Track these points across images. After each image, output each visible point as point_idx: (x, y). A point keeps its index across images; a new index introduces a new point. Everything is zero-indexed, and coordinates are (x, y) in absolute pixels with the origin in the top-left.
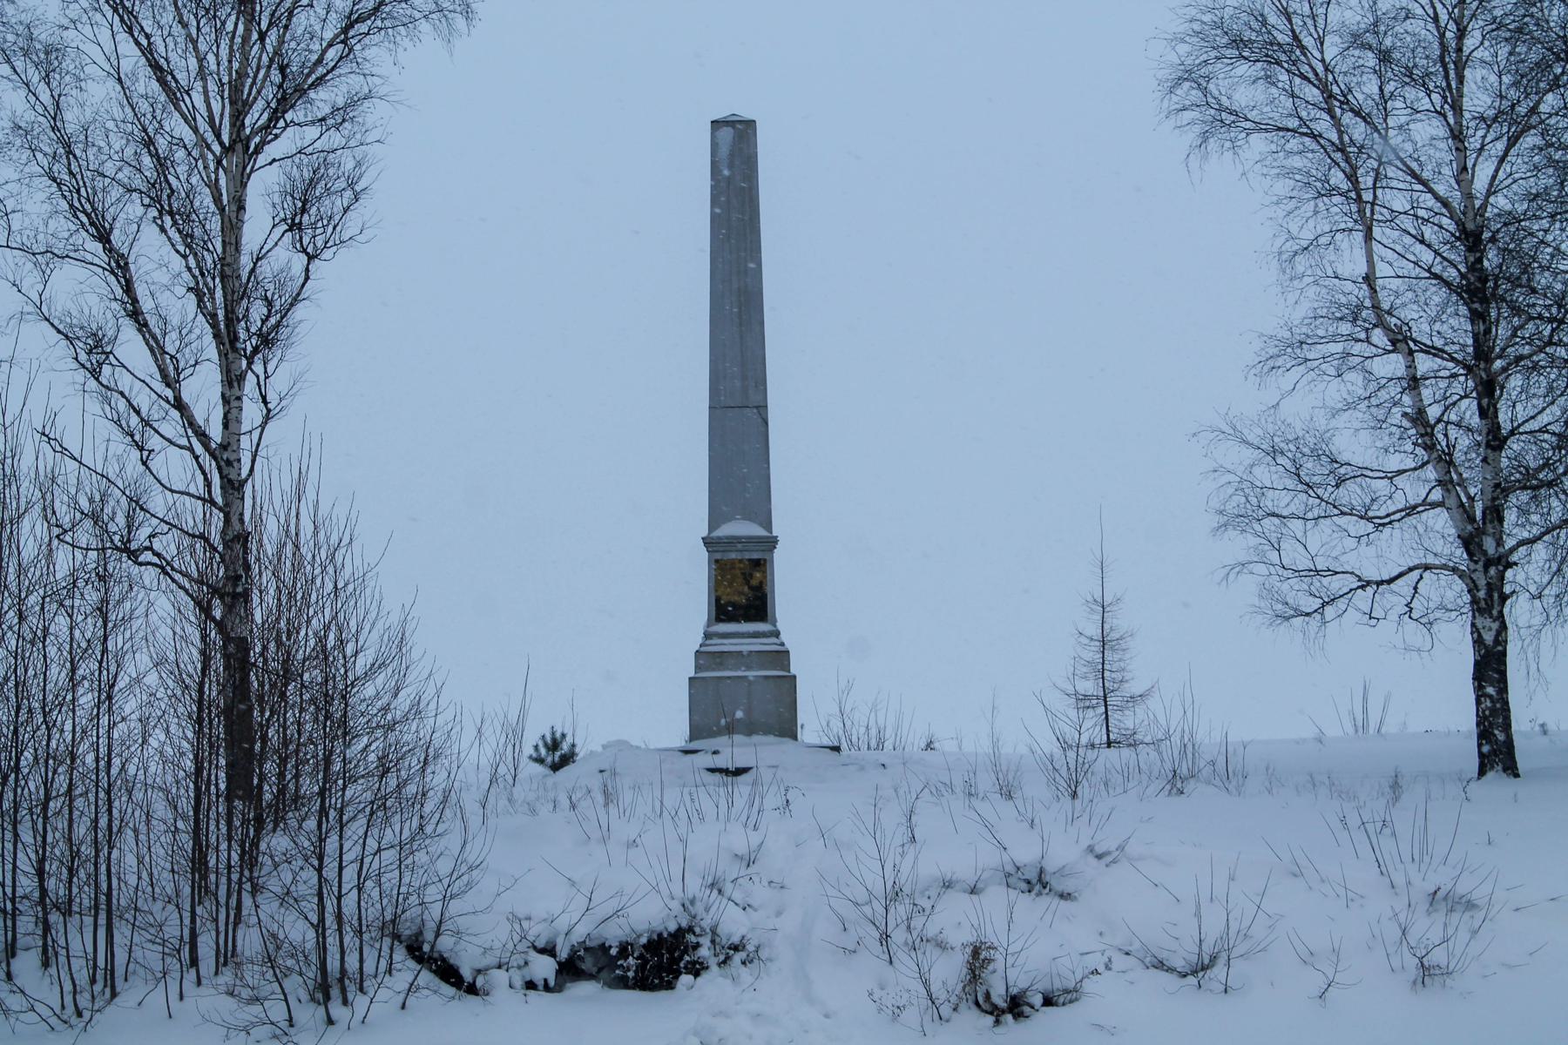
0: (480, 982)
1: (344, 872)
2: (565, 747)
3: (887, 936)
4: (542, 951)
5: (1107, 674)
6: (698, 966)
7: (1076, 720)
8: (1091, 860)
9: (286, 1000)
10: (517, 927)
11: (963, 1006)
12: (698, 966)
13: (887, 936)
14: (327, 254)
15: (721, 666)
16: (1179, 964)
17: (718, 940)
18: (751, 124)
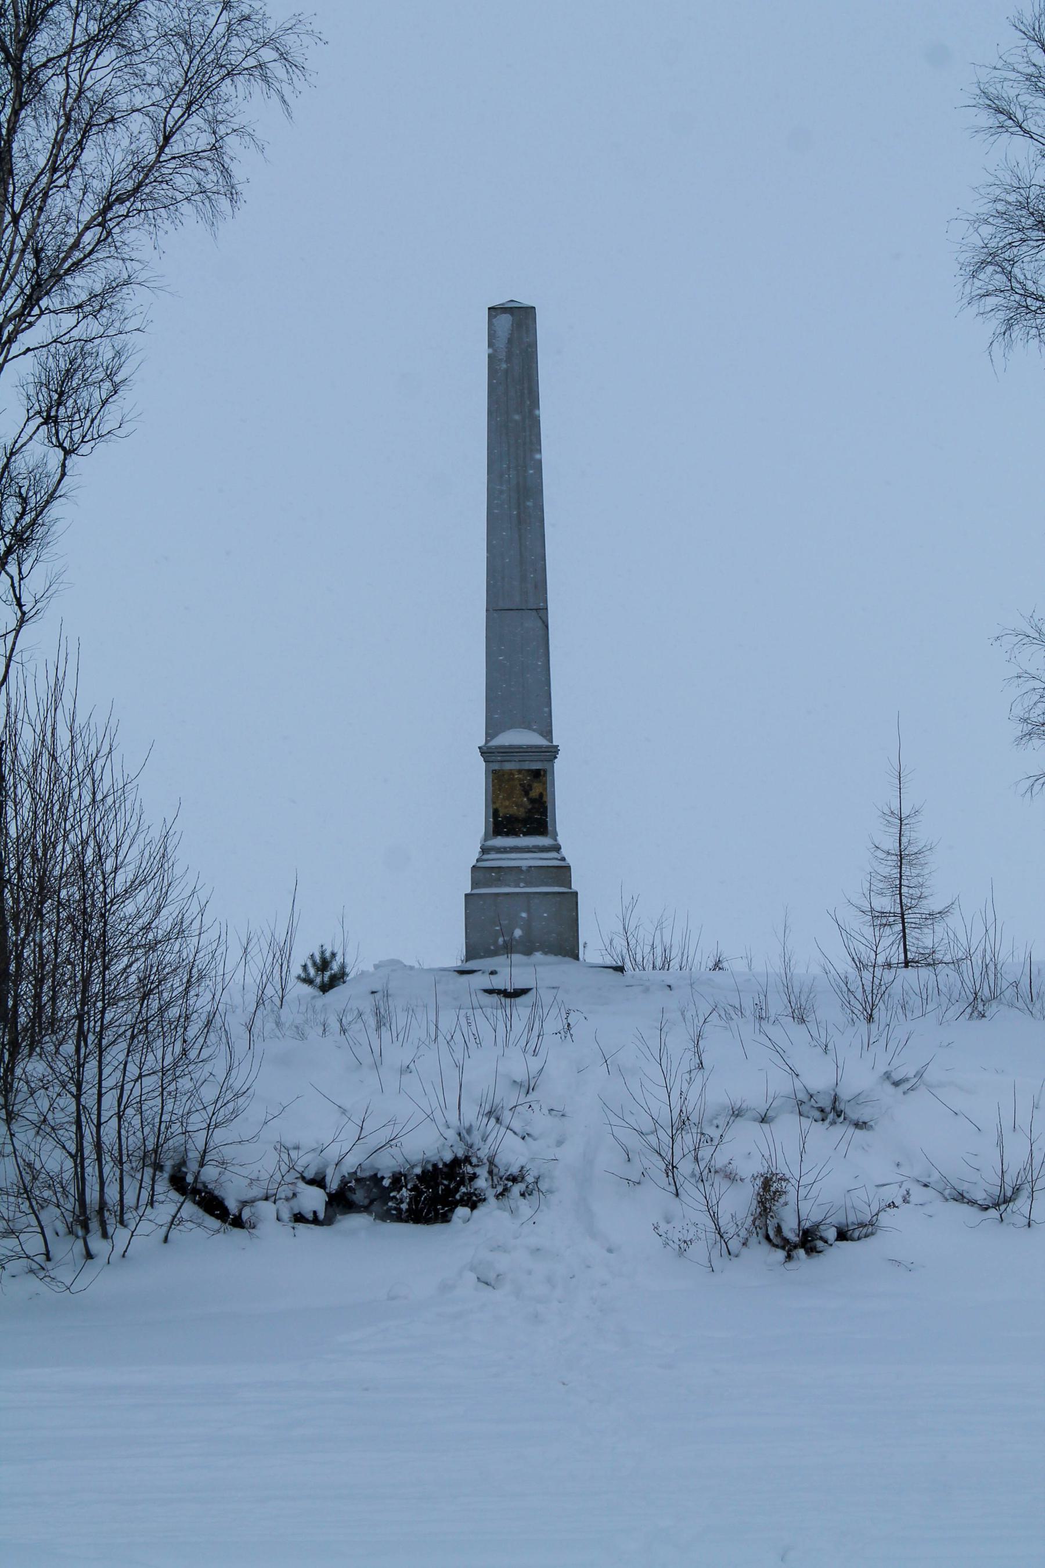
2: (335, 967)
3: (673, 1167)
4: (311, 1182)
5: (904, 890)
6: (474, 1198)
9: (43, 1233)
10: (285, 1157)
12: (474, 1198)
13: (673, 1167)
14: (85, 449)
15: (498, 882)
16: (980, 1196)
17: (495, 1170)
18: (528, 312)
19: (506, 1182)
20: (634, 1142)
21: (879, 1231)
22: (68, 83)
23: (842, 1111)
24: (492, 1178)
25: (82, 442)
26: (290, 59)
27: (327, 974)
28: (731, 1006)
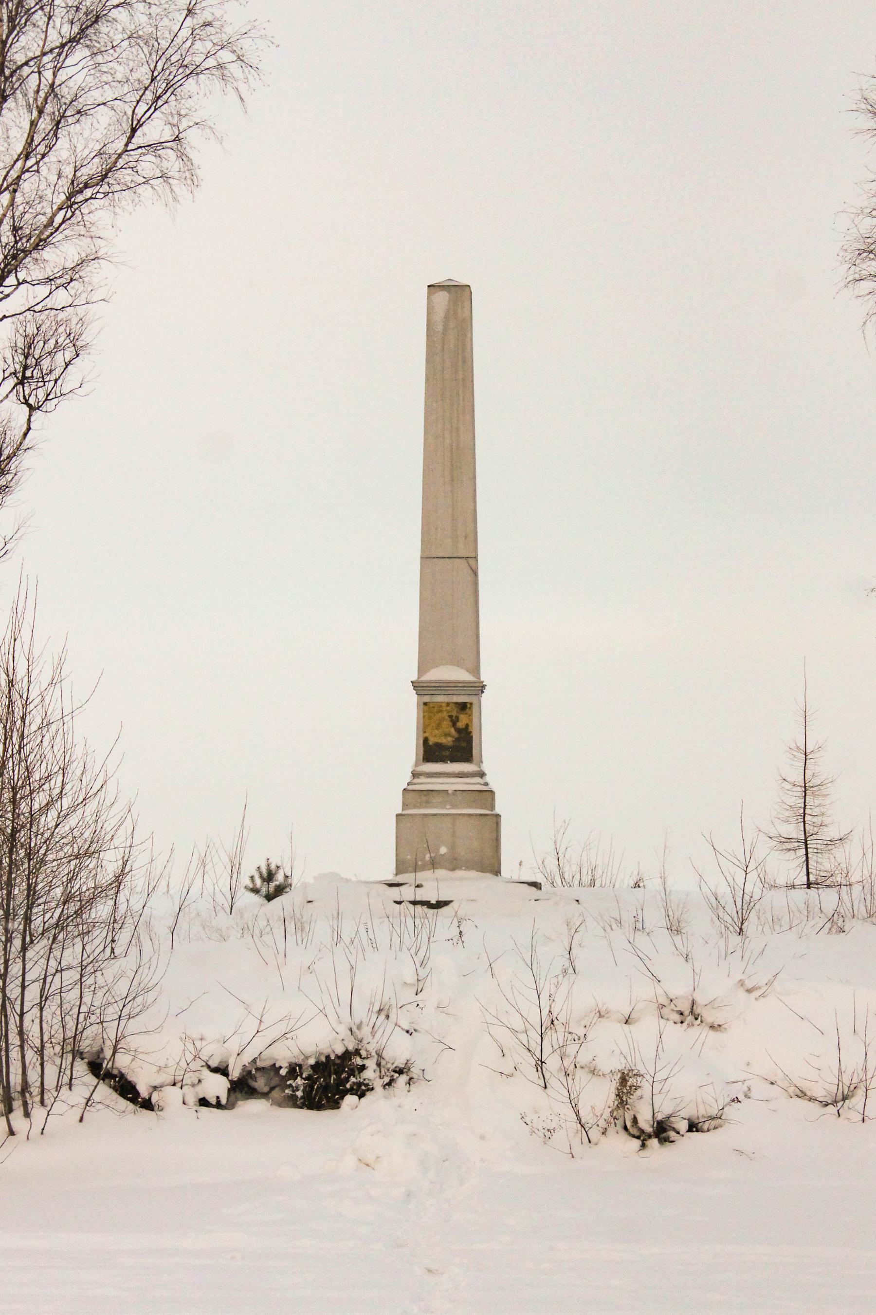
0: (154, 1100)
1: (26, 992)
2: (280, 878)
3: (542, 1062)
4: (215, 1070)
5: (808, 818)
6: (363, 1088)
7: (743, 860)
8: (742, 994)
10: (190, 1047)
11: (611, 1130)
12: (363, 1088)
13: (542, 1062)
14: (49, 405)
15: (427, 804)
16: (819, 1092)
17: (383, 1063)
18: (465, 289)
19: (393, 1073)
20: (508, 1040)
21: (727, 1124)
22: (40, 80)
23: (699, 1015)
24: (380, 1069)
25: (46, 400)
26: (246, 61)
27: (272, 885)
28: (613, 918)
